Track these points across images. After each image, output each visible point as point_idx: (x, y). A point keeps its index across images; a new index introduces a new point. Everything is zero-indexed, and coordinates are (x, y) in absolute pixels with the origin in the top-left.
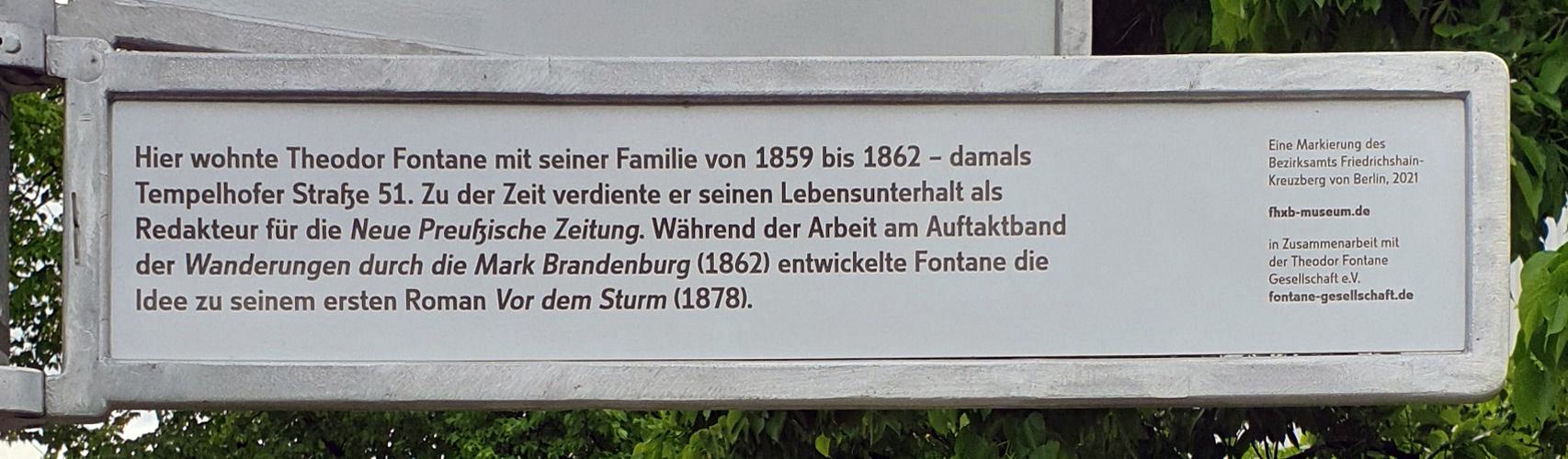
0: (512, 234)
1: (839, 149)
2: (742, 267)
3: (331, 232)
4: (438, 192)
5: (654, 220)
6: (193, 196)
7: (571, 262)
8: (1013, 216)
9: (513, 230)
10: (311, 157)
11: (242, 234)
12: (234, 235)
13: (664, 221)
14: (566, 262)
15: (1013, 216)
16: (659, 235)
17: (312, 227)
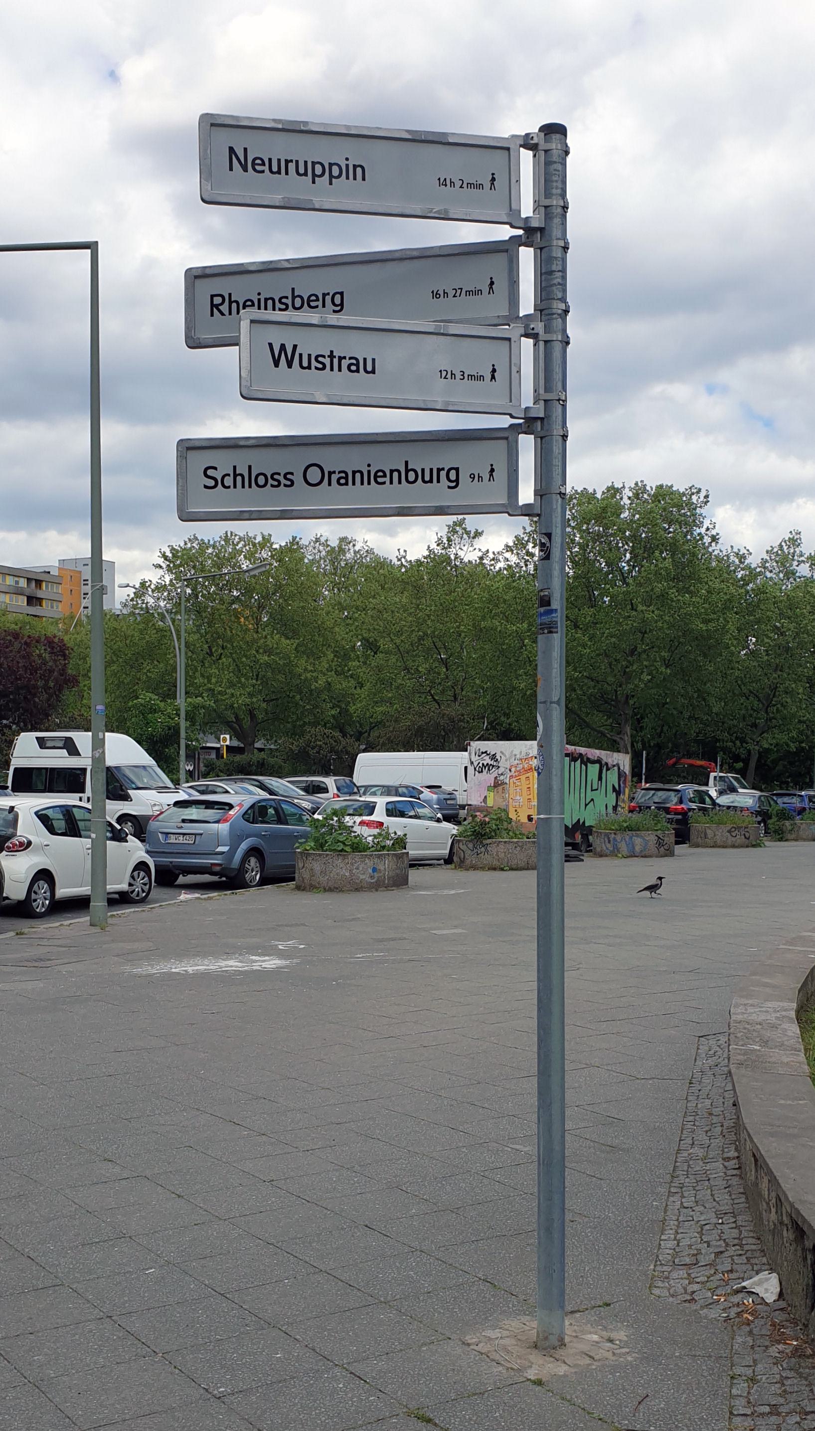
0: (226, 484)
1: (259, 294)
2: (438, 296)
3: (376, 477)
4: (301, 355)
5: (270, 345)
6: (335, 171)
7: (339, 472)
8: (230, 295)
9: (226, 478)
10: (237, 302)
11: (275, 169)
12: (266, 168)
13: (283, 347)
14: (334, 472)
15: (230, 295)
16: (276, 363)
17: (320, 176)
